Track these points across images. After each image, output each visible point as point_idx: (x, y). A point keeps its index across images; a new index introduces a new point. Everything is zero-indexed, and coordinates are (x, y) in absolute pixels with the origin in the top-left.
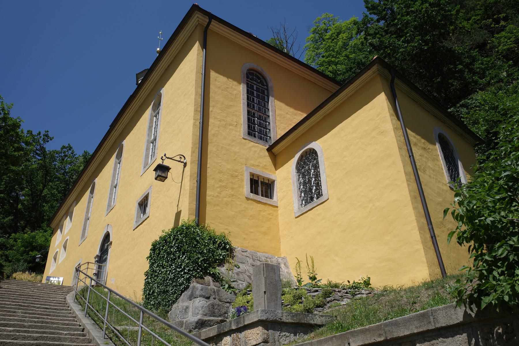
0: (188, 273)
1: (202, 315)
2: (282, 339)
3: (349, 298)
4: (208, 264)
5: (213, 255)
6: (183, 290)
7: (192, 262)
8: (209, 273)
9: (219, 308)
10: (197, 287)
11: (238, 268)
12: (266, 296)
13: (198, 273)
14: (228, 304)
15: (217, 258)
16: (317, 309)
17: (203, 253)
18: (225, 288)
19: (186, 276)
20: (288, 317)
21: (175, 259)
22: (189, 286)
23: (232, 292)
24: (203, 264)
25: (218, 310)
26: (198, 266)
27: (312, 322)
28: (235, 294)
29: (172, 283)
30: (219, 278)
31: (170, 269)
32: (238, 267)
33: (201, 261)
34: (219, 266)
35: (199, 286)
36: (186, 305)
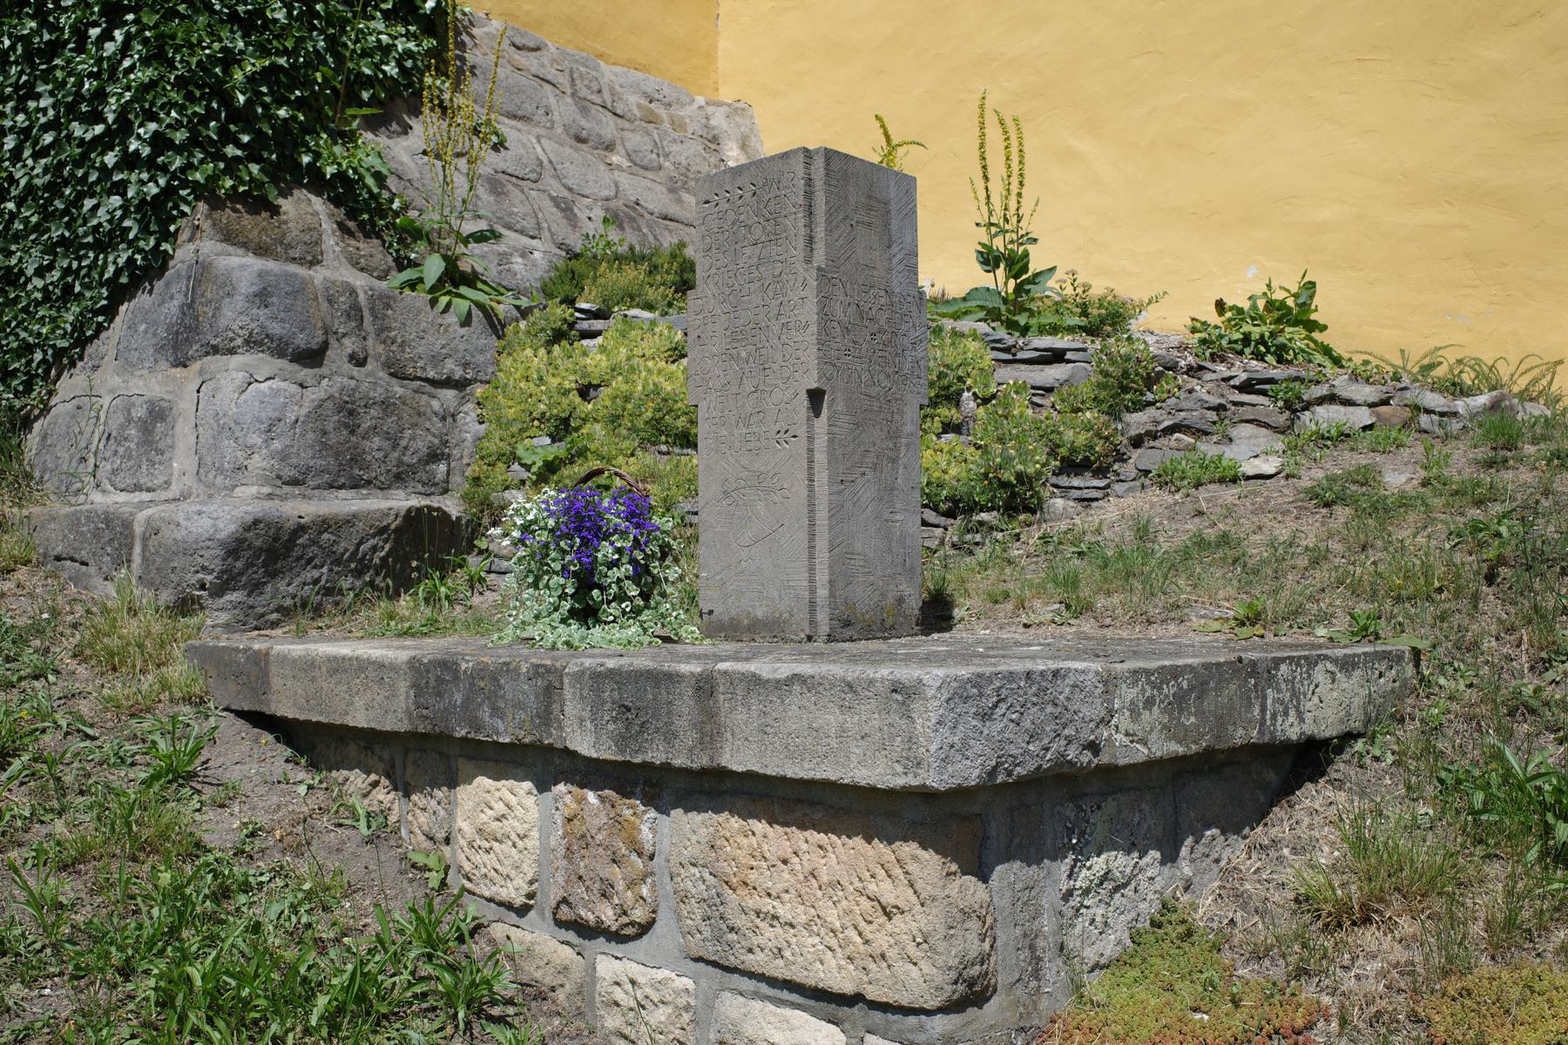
0: (151, 164)
1: (266, 481)
2: (1081, 923)
3: (1267, 426)
4: (299, 104)
5: (333, 44)
6: (124, 280)
7: (181, 83)
8: (315, 172)
9: (390, 424)
10: (229, 273)
11: (496, 148)
12: (821, 423)
13: (232, 166)
14: (449, 394)
15: (360, 74)
16: (1064, 481)
17: (265, 26)
18: (421, 280)
19: (142, 183)
20: (1146, 715)
21: (55, 48)
22: (167, 257)
23: (476, 312)
24: (265, 106)
25: (387, 436)
26: (229, 120)
27: (1291, 729)
28: (496, 326)
29: (45, 219)
30: (381, 211)
31: (21, 117)
32: (494, 139)
33: (251, 79)
34: (373, 124)
35: (242, 267)
36: (148, 395)
